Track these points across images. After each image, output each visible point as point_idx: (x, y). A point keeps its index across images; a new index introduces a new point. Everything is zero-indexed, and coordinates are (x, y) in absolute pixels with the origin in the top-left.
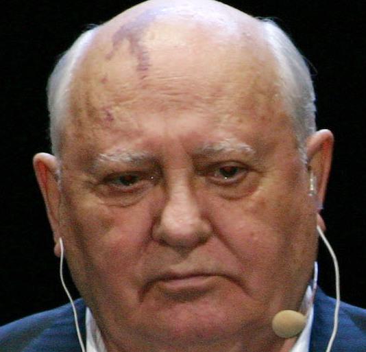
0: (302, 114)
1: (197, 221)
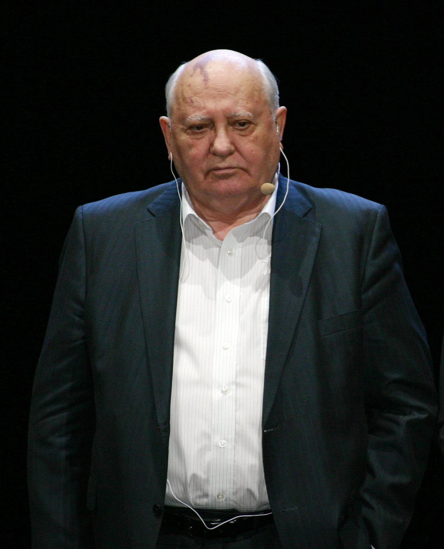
1: (229, 145)
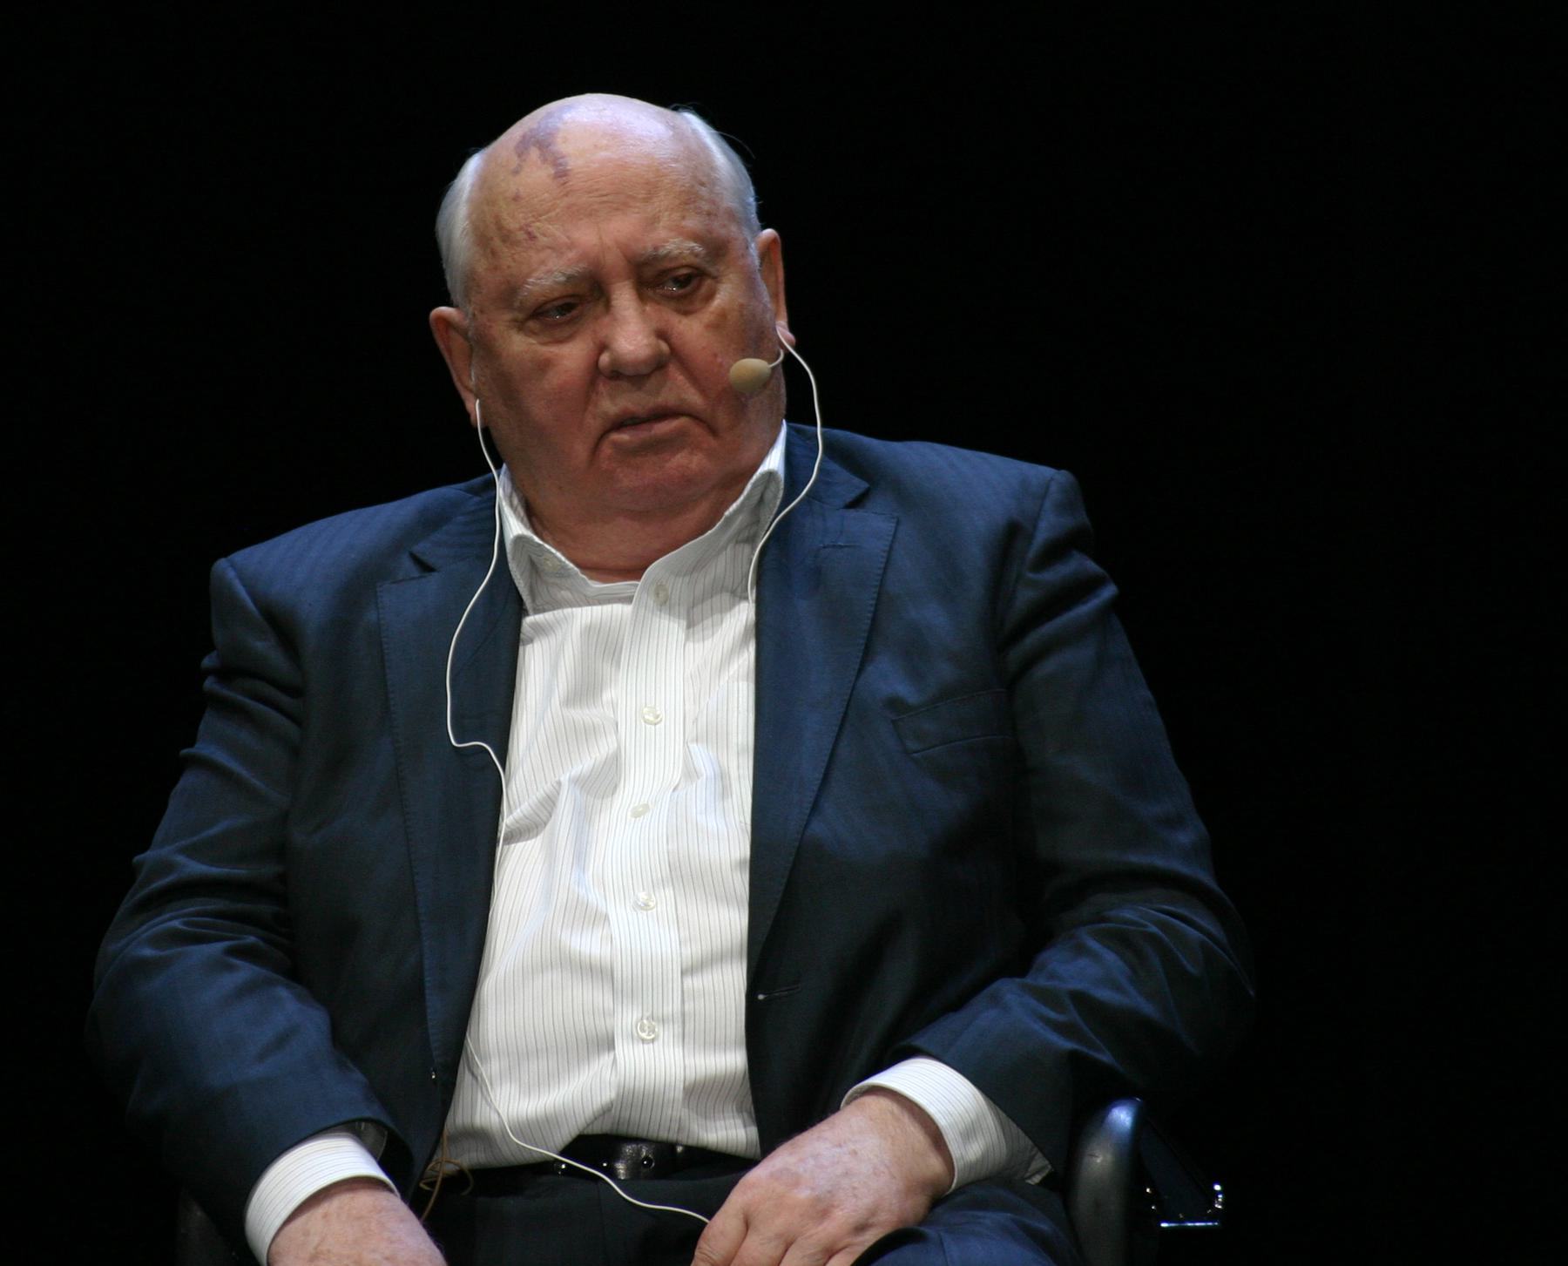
0: (745, 205)
1: (653, 340)
